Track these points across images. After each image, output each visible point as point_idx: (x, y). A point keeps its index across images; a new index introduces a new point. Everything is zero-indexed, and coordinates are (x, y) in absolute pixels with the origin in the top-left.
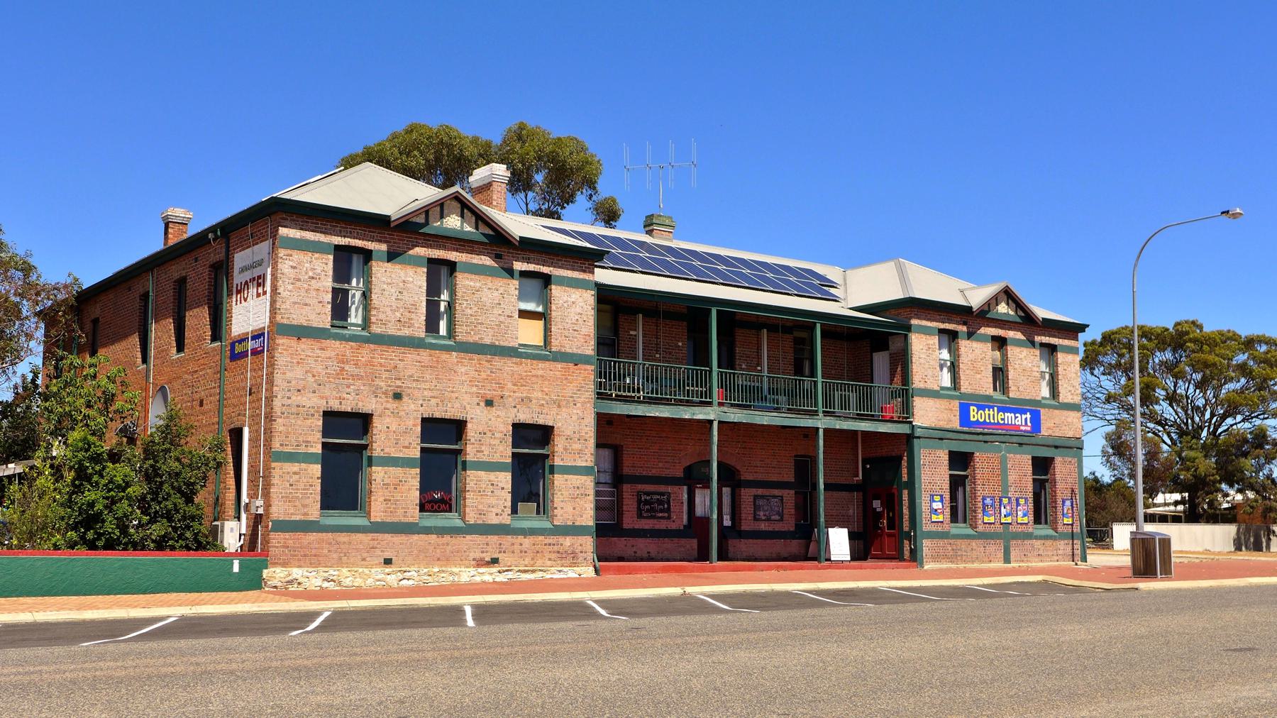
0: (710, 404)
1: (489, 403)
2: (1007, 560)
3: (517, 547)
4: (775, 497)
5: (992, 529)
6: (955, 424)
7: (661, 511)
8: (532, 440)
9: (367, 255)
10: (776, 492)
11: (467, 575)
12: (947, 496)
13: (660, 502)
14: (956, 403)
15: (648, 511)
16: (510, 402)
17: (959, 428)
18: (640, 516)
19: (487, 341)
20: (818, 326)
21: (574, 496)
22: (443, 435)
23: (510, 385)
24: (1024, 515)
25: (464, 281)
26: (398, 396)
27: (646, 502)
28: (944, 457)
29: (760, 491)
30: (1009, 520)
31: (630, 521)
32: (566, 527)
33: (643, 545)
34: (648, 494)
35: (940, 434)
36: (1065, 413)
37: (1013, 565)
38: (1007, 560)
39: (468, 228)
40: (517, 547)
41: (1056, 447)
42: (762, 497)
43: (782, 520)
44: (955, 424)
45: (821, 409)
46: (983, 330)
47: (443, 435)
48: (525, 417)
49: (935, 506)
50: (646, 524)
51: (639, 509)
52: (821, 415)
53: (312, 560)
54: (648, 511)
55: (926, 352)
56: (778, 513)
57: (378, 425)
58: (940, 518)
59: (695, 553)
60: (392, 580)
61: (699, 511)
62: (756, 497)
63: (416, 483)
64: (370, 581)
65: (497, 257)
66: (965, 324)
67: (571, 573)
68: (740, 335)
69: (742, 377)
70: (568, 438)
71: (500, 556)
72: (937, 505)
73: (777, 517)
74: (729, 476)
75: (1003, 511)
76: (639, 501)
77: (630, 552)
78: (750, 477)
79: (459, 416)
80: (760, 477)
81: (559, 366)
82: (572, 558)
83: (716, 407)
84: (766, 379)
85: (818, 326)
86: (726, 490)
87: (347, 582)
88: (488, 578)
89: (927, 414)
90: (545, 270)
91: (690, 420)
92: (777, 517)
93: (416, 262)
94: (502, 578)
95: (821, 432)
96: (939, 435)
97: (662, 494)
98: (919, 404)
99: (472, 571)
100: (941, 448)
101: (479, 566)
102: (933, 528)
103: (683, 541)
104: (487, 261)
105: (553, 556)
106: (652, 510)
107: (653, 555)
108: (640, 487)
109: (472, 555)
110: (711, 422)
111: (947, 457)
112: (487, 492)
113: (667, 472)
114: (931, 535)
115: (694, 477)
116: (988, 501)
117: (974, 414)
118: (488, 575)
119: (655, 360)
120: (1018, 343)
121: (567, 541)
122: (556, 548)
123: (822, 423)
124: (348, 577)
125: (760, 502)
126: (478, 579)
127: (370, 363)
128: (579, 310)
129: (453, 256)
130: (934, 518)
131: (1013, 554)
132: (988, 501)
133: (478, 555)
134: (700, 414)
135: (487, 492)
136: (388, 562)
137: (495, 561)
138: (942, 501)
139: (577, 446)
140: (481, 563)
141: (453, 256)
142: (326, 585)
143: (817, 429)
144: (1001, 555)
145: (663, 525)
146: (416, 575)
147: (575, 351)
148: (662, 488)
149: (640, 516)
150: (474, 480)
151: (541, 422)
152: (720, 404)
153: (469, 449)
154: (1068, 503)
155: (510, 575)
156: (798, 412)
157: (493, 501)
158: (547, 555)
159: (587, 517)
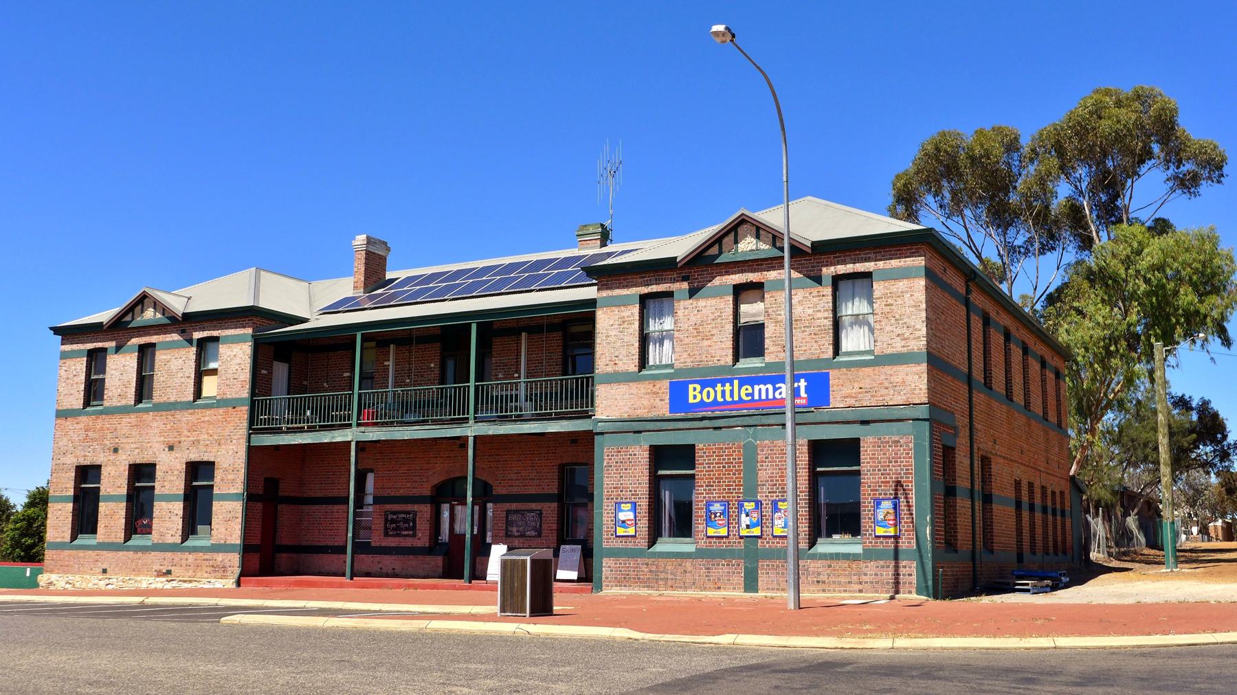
0: (350, 425)
1: (171, 448)
2: (751, 584)
3: (184, 562)
4: (532, 511)
5: (723, 545)
6: (663, 409)
7: (407, 529)
8: (199, 473)
9: (104, 351)
10: (533, 506)
11: (145, 582)
12: (644, 504)
13: (406, 521)
14: (666, 384)
15: (394, 529)
16: (184, 445)
17: (668, 415)
18: (386, 534)
19: (172, 400)
20: (474, 327)
21: (228, 519)
22: (142, 473)
23: (186, 432)
24: (787, 521)
25: (160, 356)
26: (116, 450)
27: (393, 521)
28: (643, 456)
29: (514, 506)
30: (756, 531)
31: (377, 540)
32: (220, 545)
33: (388, 562)
34: (394, 513)
35: (637, 426)
36: (888, 369)
37: (761, 594)
38: (751, 584)
39: (763, 246)
40: (184, 562)
41: (865, 423)
42: (516, 512)
43: (539, 535)
44: (663, 409)
45: (471, 415)
46: (717, 281)
47: (142, 473)
48: (194, 456)
49: (622, 516)
50: (392, 542)
51: (386, 528)
52: (471, 422)
53: (64, 569)
54: (394, 529)
55: (615, 330)
56: (535, 529)
57: (104, 472)
58: (631, 531)
59: (440, 570)
60: (102, 584)
61: (458, 529)
62: (508, 512)
63: (123, 513)
64: (90, 585)
65: (182, 332)
66: (684, 279)
67: (218, 584)
68: (497, 343)
69: (496, 386)
70: (226, 470)
71: (173, 569)
72: (626, 515)
73: (534, 533)
74: (484, 494)
75: (745, 520)
76: (386, 520)
77: (376, 569)
78: (503, 491)
79: (151, 461)
80: (515, 490)
81: (221, 411)
82: (221, 571)
83: (354, 428)
84: (523, 385)
85: (474, 327)
86: (476, 508)
87: (77, 585)
88: (160, 586)
89: (612, 403)
90: (861, 267)
91: (493, 436)
92: (534, 533)
93: (718, 293)
94: (168, 586)
95: (471, 440)
96: (633, 427)
97: (409, 513)
98: (603, 394)
99: (151, 580)
100: (638, 443)
101: (158, 576)
102: (619, 544)
103: (428, 558)
104: (175, 337)
105: (209, 569)
106: (398, 528)
107: (397, 571)
108: (388, 507)
109: (155, 567)
110: (349, 443)
111: (646, 454)
112: (168, 516)
113: (414, 491)
114: (614, 553)
115: (449, 491)
116: (717, 508)
117: (694, 394)
118: (160, 583)
119: (407, 385)
120: (170, 346)
121: (220, 557)
122: (211, 563)
123: (471, 430)
124: (79, 581)
125: (514, 517)
126: (153, 586)
127: (102, 429)
128: (238, 361)
129: (154, 339)
130: (620, 531)
131: (762, 580)
132: (717, 508)
133: (157, 567)
134: (338, 436)
135: (168, 516)
136: (105, 571)
137: (169, 572)
138: (634, 509)
139: (231, 477)
140: (160, 574)
141: (154, 339)
142: (68, 586)
143: (467, 437)
144: (739, 579)
145: (408, 542)
146: (116, 582)
147: (234, 396)
148: (409, 507)
149: (386, 534)
150: (159, 508)
151: (205, 459)
152: (359, 425)
153: (157, 485)
154: (887, 505)
155: (174, 584)
156: (442, 422)
157: (168, 525)
158: (205, 569)
159: (236, 538)
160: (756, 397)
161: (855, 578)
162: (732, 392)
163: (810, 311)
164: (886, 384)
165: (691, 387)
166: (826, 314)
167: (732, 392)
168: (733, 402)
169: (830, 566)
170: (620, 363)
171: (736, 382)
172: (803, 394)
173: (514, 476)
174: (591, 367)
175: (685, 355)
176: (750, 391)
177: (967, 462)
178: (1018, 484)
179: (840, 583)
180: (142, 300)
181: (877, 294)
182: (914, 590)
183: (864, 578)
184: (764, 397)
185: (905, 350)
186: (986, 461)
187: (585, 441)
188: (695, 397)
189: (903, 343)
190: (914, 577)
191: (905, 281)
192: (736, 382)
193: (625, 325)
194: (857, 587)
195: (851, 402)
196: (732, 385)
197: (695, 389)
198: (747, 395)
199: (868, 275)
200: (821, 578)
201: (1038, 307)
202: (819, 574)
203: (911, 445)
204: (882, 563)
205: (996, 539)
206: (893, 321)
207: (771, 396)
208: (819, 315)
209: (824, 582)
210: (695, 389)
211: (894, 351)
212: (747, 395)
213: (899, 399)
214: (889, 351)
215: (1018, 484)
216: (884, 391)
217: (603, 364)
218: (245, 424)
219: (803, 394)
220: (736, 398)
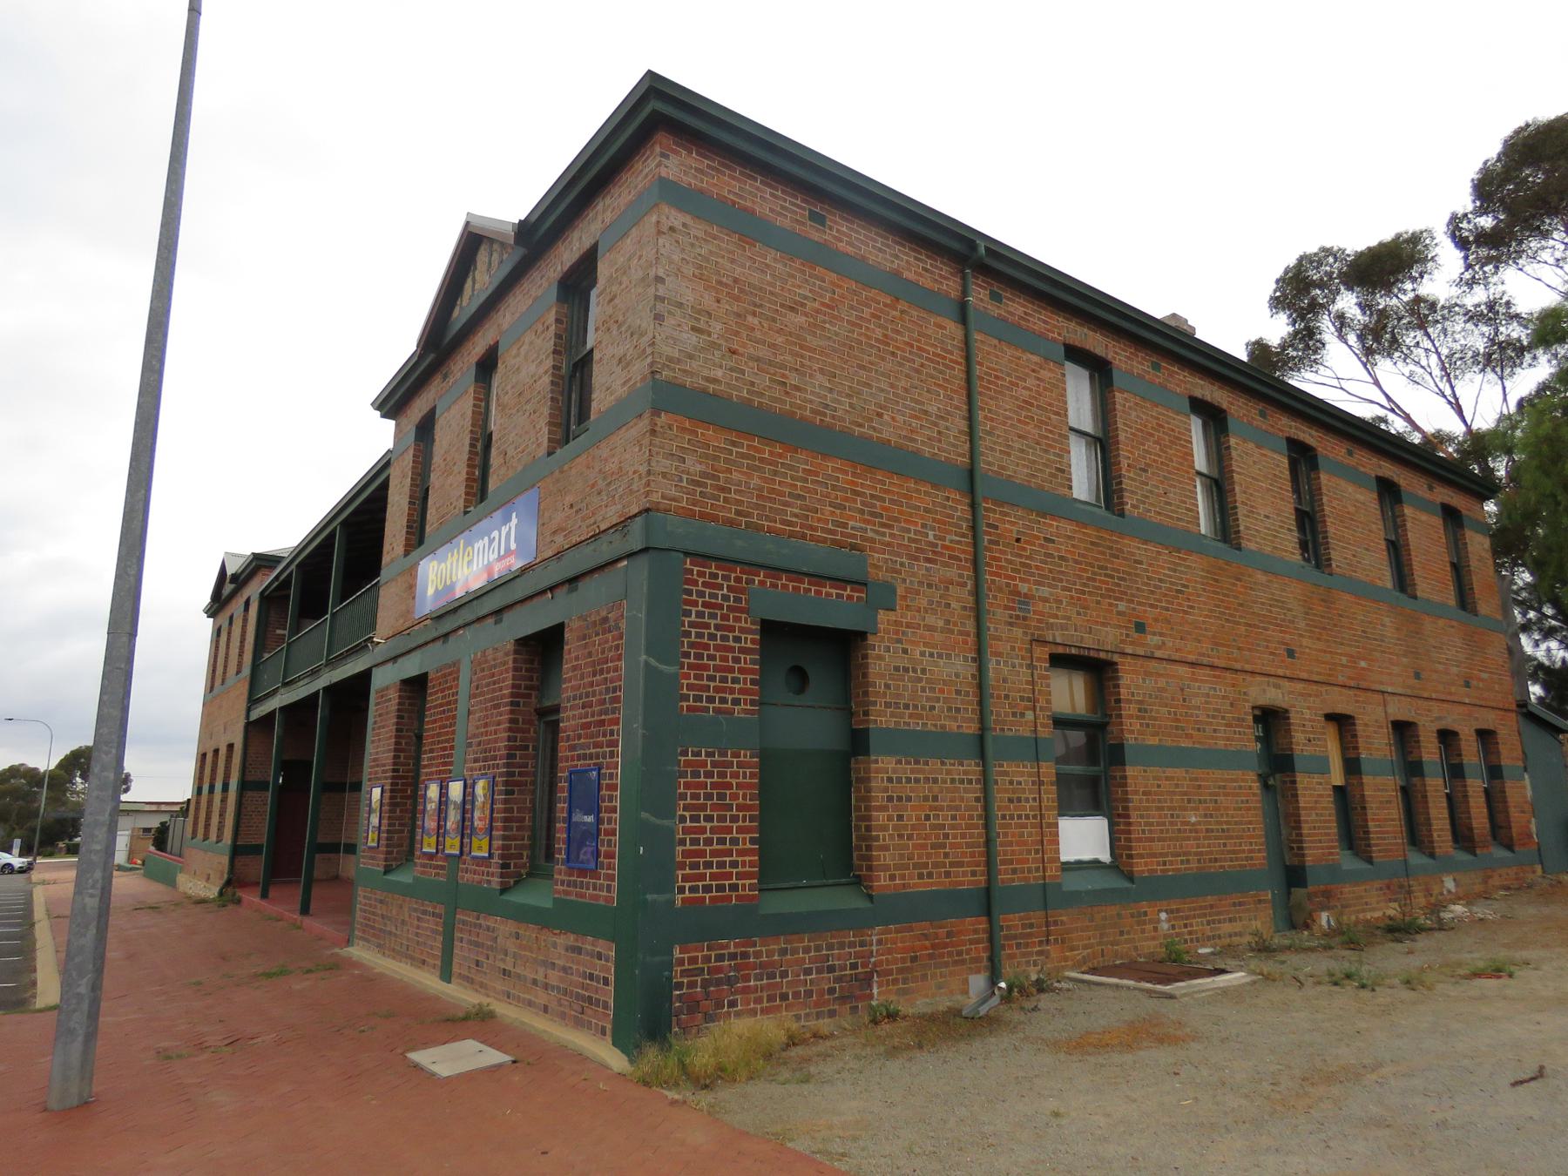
199: (589, 260)
215: (1270, 719)
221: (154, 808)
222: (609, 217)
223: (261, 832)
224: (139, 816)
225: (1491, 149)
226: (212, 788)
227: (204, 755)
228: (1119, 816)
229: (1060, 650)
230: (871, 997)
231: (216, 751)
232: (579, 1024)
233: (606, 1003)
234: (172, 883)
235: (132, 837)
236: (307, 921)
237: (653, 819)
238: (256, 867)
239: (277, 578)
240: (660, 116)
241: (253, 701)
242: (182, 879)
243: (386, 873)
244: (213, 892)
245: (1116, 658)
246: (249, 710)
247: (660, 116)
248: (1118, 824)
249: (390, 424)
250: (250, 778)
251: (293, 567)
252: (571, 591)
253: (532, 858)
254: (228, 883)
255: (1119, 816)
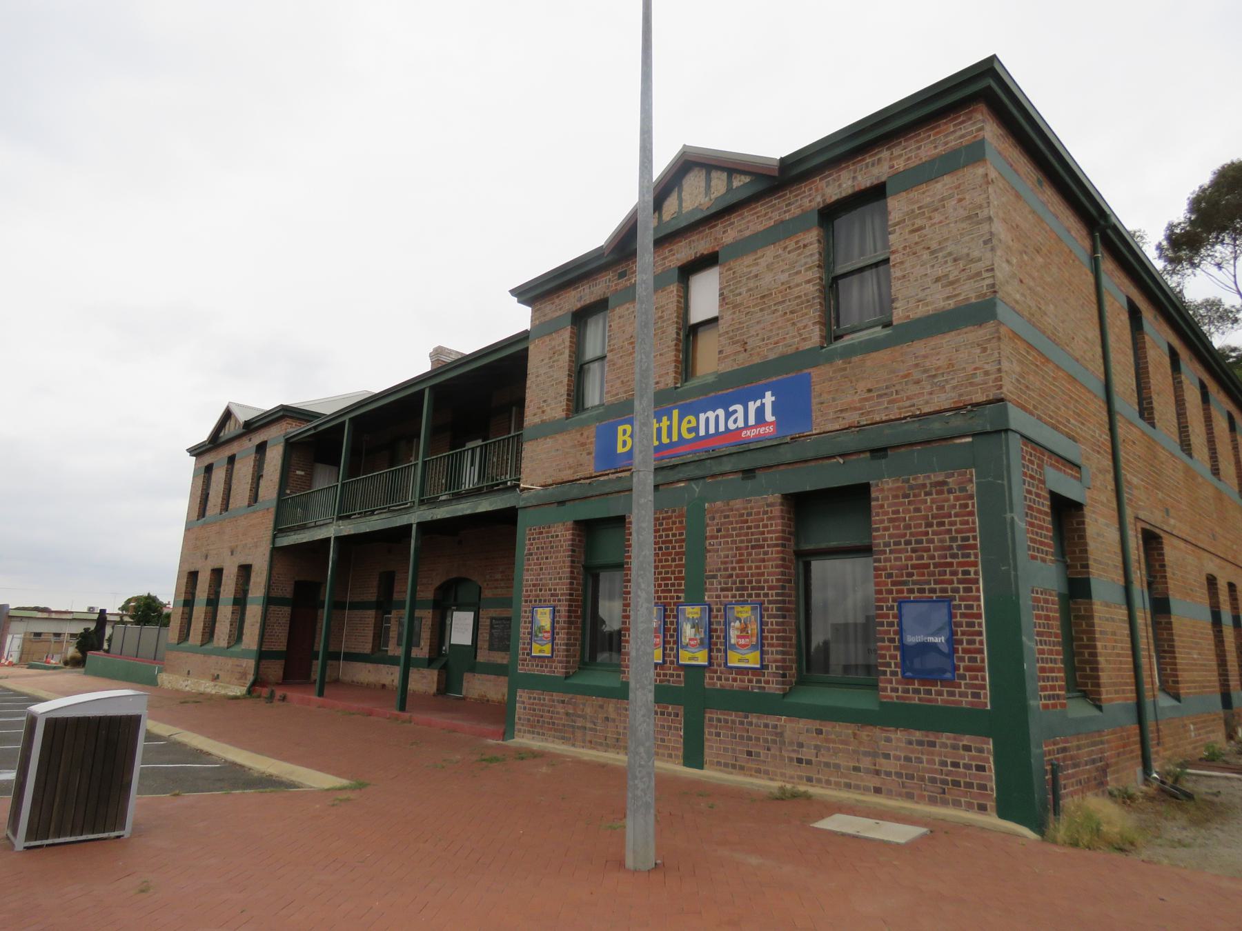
37: (709, 774)
131: (712, 748)
160: (702, 433)
161: (866, 763)
162: (670, 428)
163: (784, 277)
164: (917, 375)
165: (620, 429)
166: (810, 275)
167: (670, 428)
168: (672, 444)
169: (819, 732)
170: (548, 409)
171: (675, 413)
172: (769, 417)
173: (499, 576)
174: (520, 424)
175: (618, 383)
176: (694, 424)
177: (1113, 535)
178: (1211, 581)
179: (837, 766)
180: (228, 415)
181: (894, 216)
182: (991, 804)
183: (885, 765)
184: (712, 430)
185: (951, 304)
186: (1151, 540)
187: (508, 517)
188: (625, 443)
189: (949, 291)
190: (991, 772)
191: (947, 179)
192: (675, 413)
193: (556, 357)
194: (873, 782)
195: (853, 418)
196: (670, 419)
197: (625, 431)
198: (690, 430)
199: (877, 193)
200: (807, 753)
201: (1213, 330)
202: (801, 745)
203: (972, 488)
204: (918, 735)
205: (1183, 676)
206: (926, 256)
207: (722, 428)
208: (798, 279)
209: (809, 762)
210: (625, 431)
211: (930, 310)
212: (690, 430)
213: (942, 400)
214: (921, 311)
215: (1211, 581)
216: (913, 389)
217: (531, 417)
218: (271, 525)
219: (769, 417)
220: (675, 438)
221: (45, 615)
222: (900, 165)
223: (280, 643)
224: (32, 622)
225: (1204, 177)
226: (213, 602)
227: (193, 576)
228: (1165, 651)
229: (1148, 527)
230: (1107, 783)
231: (217, 573)
232: (945, 803)
233: (983, 787)
234: (151, 681)
235: (24, 640)
236: (406, 715)
237: (931, 639)
238: (275, 670)
239: (315, 427)
240: (983, 91)
241: (278, 531)
242: (166, 679)
243: (566, 678)
244: (239, 690)
245: (1162, 534)
246: (275, 537)
247: (983, 91)
248: (1164, 658)
249: (527, 311)
250: (273, 594)
251: (346, 418)
252: (873, 458)
253: (799, 669)
254: (254, 684)
255: (1165, 651)
